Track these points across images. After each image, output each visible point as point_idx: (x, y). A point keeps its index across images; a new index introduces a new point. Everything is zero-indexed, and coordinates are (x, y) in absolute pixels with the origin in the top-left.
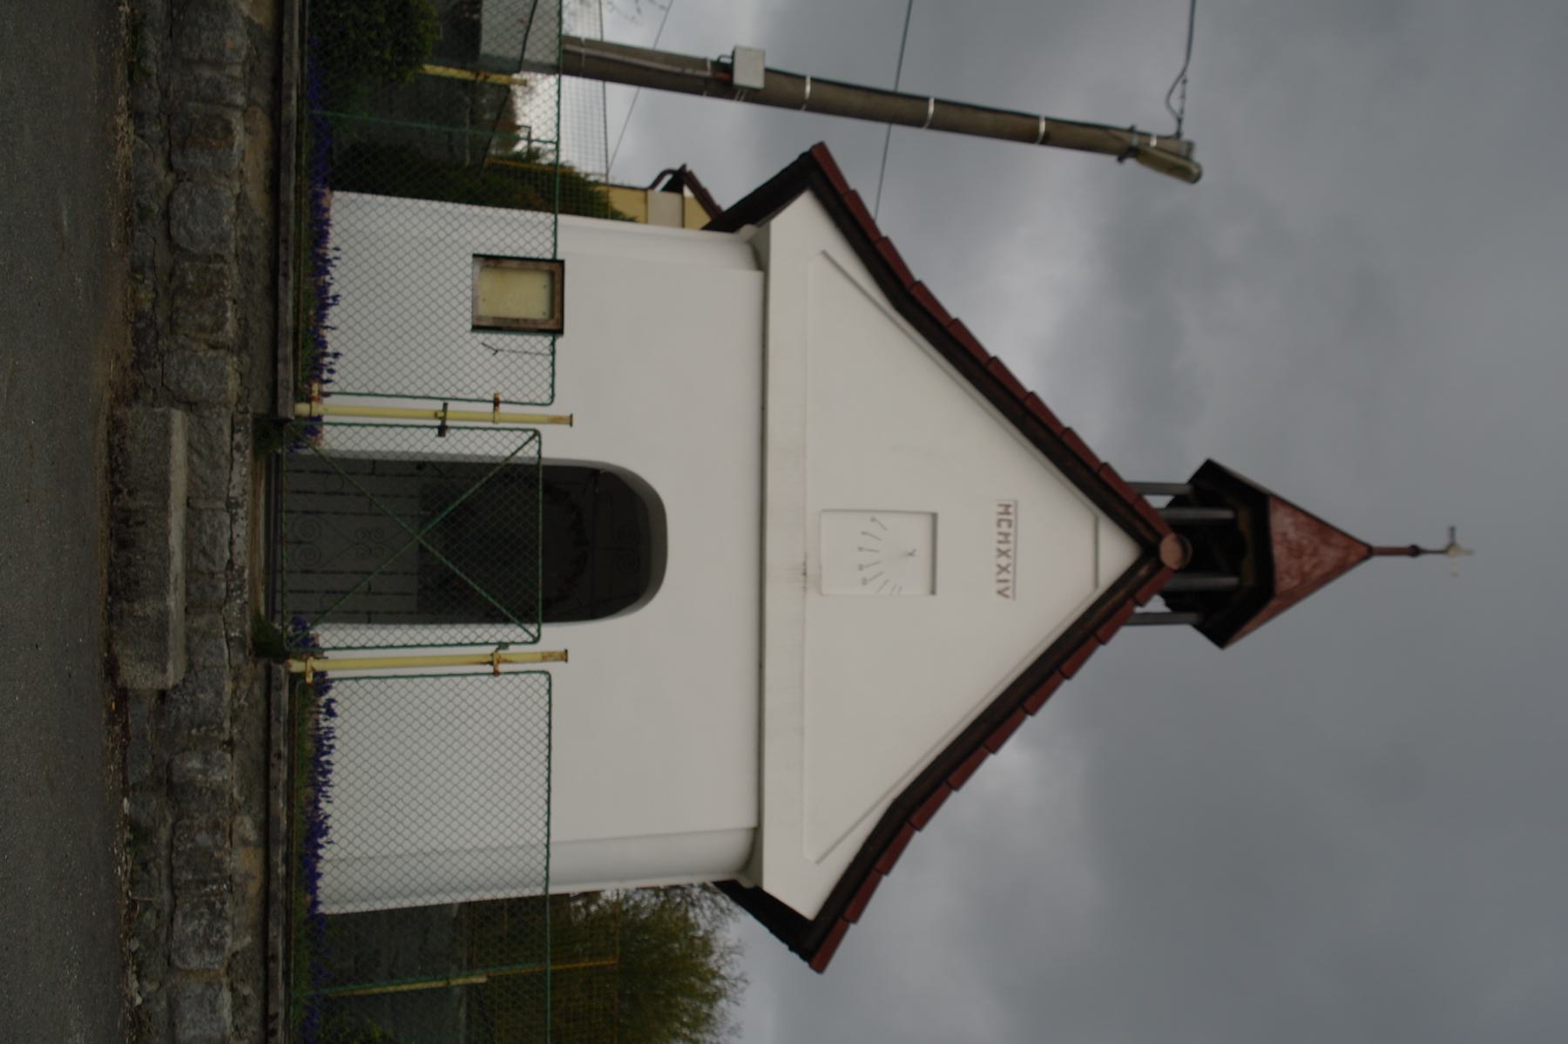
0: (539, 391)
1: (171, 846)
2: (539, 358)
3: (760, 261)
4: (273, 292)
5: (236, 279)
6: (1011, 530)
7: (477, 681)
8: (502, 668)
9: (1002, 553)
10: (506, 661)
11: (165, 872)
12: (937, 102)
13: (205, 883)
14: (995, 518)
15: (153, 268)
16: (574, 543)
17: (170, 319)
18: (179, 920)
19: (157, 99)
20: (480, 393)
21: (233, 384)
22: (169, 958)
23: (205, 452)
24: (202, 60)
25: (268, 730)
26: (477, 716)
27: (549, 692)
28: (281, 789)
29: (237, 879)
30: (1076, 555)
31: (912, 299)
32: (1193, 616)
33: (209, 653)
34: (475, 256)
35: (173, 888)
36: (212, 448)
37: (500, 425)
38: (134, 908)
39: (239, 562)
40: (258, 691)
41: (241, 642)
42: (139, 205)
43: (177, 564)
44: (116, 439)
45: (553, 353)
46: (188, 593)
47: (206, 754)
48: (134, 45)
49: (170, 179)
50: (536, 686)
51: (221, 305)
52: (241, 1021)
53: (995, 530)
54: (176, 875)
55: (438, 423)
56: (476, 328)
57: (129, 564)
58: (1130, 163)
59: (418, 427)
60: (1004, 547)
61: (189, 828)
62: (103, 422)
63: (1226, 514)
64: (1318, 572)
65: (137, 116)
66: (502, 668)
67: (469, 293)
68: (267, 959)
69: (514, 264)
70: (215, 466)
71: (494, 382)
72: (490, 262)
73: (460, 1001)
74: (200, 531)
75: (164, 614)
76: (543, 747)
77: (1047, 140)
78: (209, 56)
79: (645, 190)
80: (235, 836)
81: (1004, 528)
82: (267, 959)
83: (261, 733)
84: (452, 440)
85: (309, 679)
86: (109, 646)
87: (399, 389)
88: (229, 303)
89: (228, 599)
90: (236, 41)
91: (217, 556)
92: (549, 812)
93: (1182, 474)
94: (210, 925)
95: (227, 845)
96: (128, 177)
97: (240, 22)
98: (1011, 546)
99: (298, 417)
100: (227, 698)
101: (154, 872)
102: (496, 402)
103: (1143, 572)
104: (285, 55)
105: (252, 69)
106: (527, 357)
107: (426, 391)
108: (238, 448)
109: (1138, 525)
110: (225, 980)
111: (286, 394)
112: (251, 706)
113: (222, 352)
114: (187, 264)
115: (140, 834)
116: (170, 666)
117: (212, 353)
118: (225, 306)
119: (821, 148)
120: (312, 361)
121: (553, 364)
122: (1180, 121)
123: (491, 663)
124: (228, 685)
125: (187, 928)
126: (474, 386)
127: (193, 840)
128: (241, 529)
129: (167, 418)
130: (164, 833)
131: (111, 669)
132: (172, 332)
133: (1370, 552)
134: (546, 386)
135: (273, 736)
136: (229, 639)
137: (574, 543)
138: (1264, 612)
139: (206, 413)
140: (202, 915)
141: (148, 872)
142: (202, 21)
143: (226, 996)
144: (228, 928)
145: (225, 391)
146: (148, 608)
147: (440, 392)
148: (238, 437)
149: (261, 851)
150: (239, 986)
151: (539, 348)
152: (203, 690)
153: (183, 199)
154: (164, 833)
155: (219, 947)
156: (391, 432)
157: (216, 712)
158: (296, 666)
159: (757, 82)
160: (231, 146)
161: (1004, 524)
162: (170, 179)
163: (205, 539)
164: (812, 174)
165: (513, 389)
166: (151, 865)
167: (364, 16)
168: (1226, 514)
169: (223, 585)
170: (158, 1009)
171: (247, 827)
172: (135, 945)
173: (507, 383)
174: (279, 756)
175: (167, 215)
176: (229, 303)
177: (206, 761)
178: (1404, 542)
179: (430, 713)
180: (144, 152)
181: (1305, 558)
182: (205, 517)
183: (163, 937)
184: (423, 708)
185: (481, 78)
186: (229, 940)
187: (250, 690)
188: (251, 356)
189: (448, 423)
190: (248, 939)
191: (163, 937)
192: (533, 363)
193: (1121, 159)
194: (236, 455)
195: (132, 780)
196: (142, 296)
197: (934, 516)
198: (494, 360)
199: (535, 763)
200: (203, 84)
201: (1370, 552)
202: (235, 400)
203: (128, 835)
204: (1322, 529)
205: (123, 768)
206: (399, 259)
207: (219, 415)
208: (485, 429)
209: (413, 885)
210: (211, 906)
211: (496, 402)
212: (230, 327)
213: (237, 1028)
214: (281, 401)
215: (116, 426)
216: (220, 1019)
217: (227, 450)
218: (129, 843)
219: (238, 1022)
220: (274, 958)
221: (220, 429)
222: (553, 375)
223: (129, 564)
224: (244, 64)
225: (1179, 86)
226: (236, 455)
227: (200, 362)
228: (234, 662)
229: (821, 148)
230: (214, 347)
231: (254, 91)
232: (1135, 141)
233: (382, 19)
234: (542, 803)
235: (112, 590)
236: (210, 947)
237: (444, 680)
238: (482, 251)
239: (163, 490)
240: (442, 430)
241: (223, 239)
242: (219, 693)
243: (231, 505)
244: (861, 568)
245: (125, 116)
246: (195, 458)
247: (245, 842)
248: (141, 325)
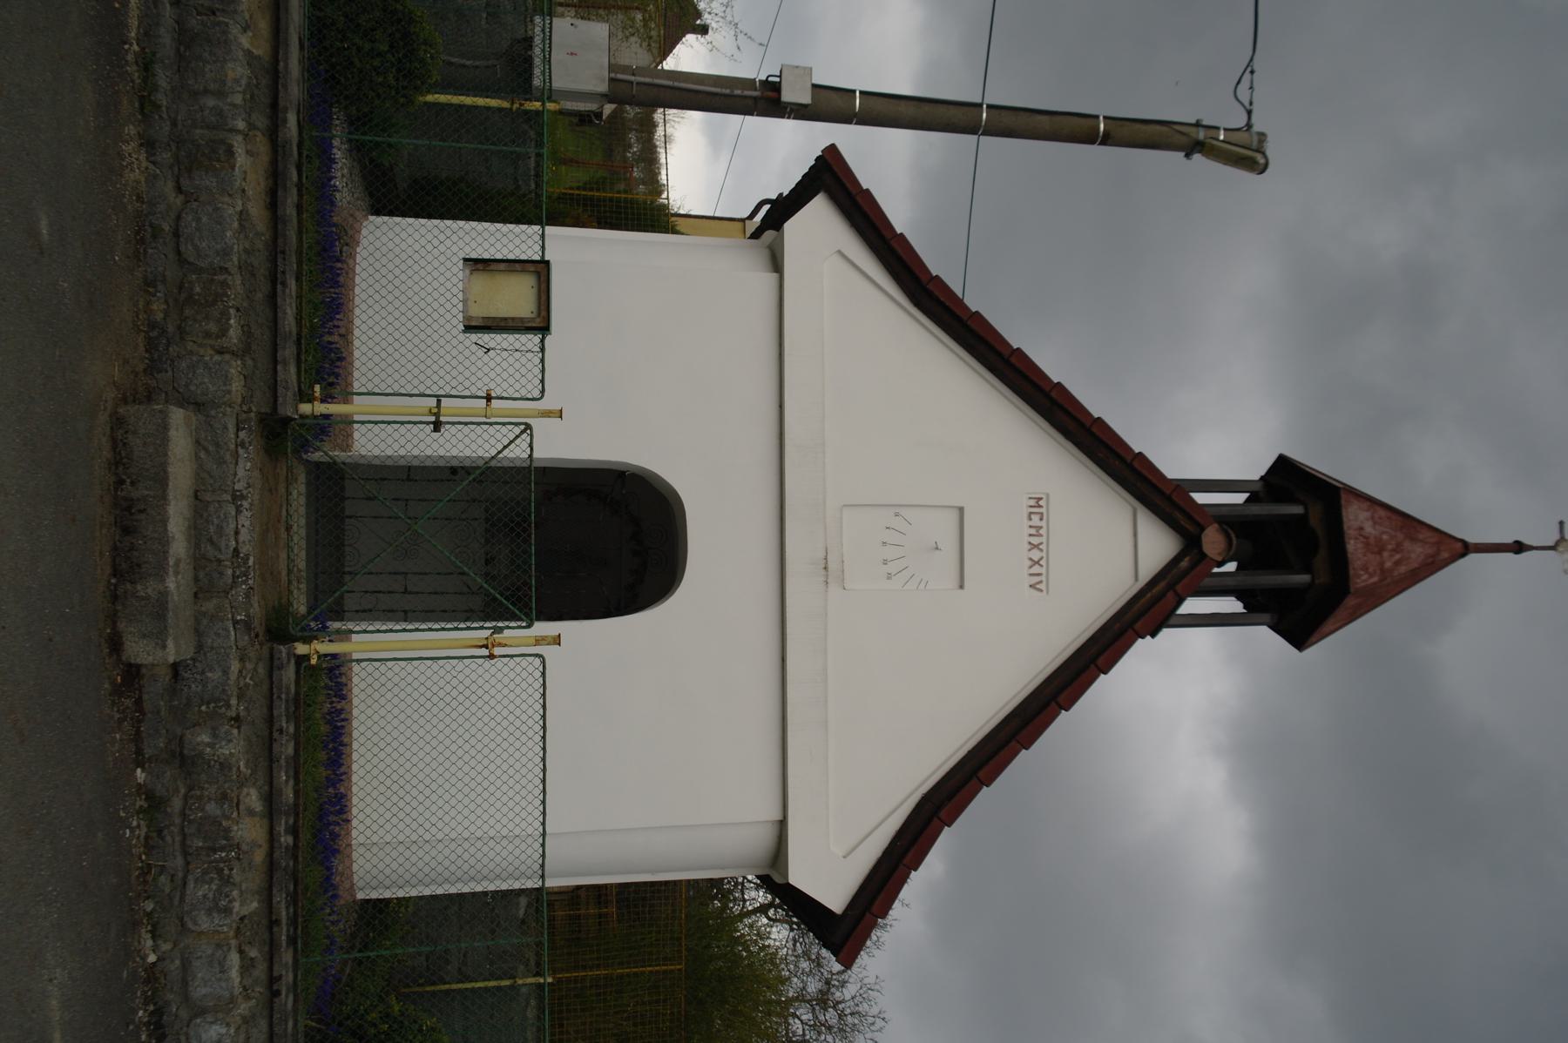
1: (183, 815)
2: (530, 355)
4: (272, 299)
5: (240, 289)
6: (1043, 523)
7: (473, 664)
8: (497, 651)
9: (1034, 546)
10: (500, 645)
11: (178, 839)
12: (989, 106)
13: (215, 851)
14: (1026, 511)
15: (164, 281)
16: (598, 543)
17: (179, 327)
18: (191, 885)
19: (167, 128)
20: (474, 390)
21: (237, 386)
22: (182, 920)
24: (206, 91)
25: (271, 708)
27: (543, 674)
28: (283, 762)
29: (244, 847)
30: (1116, 548)
31: (930, 294)
32: (1266, 617)
34: (466, 260)
35: (185, 854)
36: (217, 445)
38: (149, 872)
39: (244, 550)
40: (261, 670)
41: (247, 625)
42: (151, 225)
43: (179, 547)
45: (543, 350)
46: (196, 579)
47: (214, 729)
50: (531, 669)
51: (225, 315)
52: (248, 982)
53: (1027, 523)
55: (433, 419)
56: (469, 329)
57: (132, 548)
59: (415, 423)
60: (1035, 541)
61: (200, 798)
62: (103, 418)
63: (1297, 510)
64: (1403, 569)
65: (149, 144)
66: (497, 651)
67: (460, 296)
68: (273, 923)
69: (502, 266)
70: (221, 462)
72: (478, 265)
74: (207, 521)
75: (164, 594)
77: (1107, 140)
78: (212, 86)
79: (743, 220)
80: (242, 807)
81: (1036, 520)
83: (265, 710)
85: (314, 661)
86: (114, 623)
88: (232, 311)
89: (234, 584)
90: (237, 71)
92: (544, 791)
93: (1254, 468)
94: (219, 890)
95: (235, 814)
96: (139, 198)
97: (241, 53)
98: (1044, 539)
99: (302, 417)
100: (233, 677)
101: (169, 839)
102: (489, 398)
103: (1184, 564)
105: (252, 97)
106: (518, 355)
107: (422, 389)
108: (242, 445)
109: (1179, 516)
110: (233, 942)
112: (256, 685)
113: (227, 357)
115: (154, 803)
117: (217, 358)
119: (832, 150)
121: (542, 361)
122: (1249, 113)
124: (234, 667)
125: (199, 892)
127: (203, 810)
128: (245, 519)
129: (164, 415)
130: (177, 803)
131: (115, 644)
132: (182, 339)
133: (1466, 549)
135: (275, 713)
136: (235, 622)
137: (598, 543)
138: (1341, 612)
139: (213, 413)
141: (163, 839)
143: (234, 958)
144: (235, 893)
145: (229, 392)
146: (148, 588)
147: (435, 390)
148: (242, 434)
149: (266, 822)
150: (246, 948)
151: (530, 346)
154: (177, 803)
155: (227, 911)
156: (389, 429)
158: (301, 649)
159: (805, 98)
160: (233, 168)
161: (1035, 518)
162: (179, 200)
163: (212, 529)
164: (828, 177)
165: (505, 385)
167: (367, 46)
168: (1297, 510)
169: (230, 572)
171: (253, 798)
172: (149, 906)
173: (499, 380)
174: (281, 731)
175: (176, 234)
176: (232, 311)
177: (215, 736)
178: (1509, 540)
179: (429, 694)
180: (155, 176)
181: (1386, 554)
182: (211, 509)
183: (176, 902)
184: (422, 689)
185: (516, 106)
186: (237, 904)
187: (255, 669)
189: (442, 419)
190: (255, 904)
191: (176, 902)
192: (524, 360)
193: (1188, 156)
194: (241, 451)
195: (148, 752)
196: (155, 307)
197: (961, 510)
199: (530, 743)
201: (1466, 549)
204: (1408, 524)
206: (411, 272)
208: (479, 424)
209: (447, 874)
211: (489, 398)
212: (234, 333)
213: (245, 989)
214: (280, 400)
215: (118, 422)
219: (245, 982)
220: (277, 922)
223: (132, 548)
224: (244, 93)
225: (1247, 75)
226: (241, 451)
228: (240, 644)
229: (832, 150)
230: (220, 352)
231: (254, 116)
232: (1201, 135)
233: (384, 47)
234: (538, 781)
236: (219, 911)
237: (441, 662)
238: (474, 256)
239: (162, 480)
240: (437, 426)
241: (226, 253)
242: (226, 672)
243: (237, 497)
244: (885, 562)
246: (202, 455)
247: (251, 813)
248: (154, 334)
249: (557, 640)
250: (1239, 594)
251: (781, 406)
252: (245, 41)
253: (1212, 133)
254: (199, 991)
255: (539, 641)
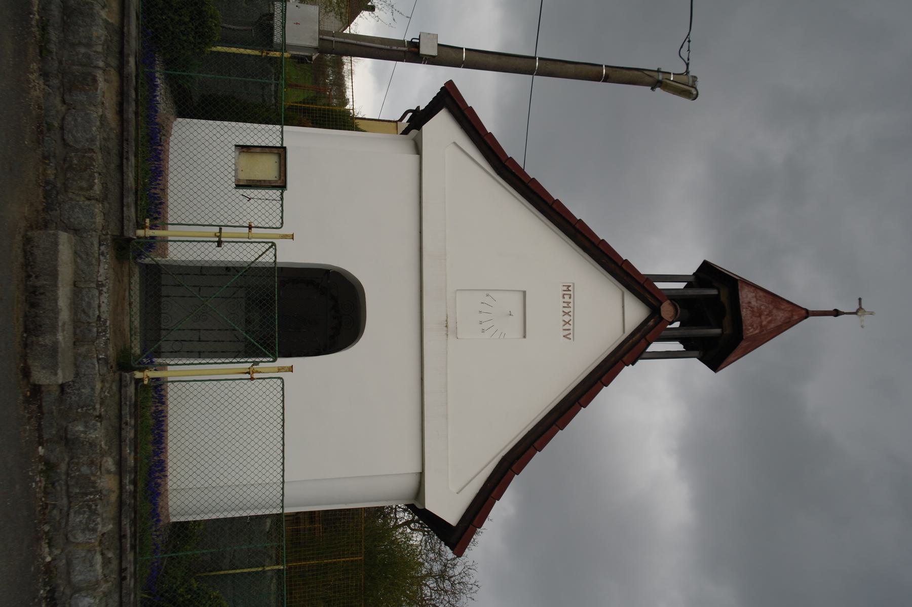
0: (274, 221)
1: (67, 474)
2: (274, 202)
3: (418, 149)
4: (120, 168)
5: (101, 162)
8: (255, 376)
9: (566, 313)
11: (64, 488)
13: (86, 494)
14: (561, 293)
15: (54, 156)
16: (313, 311)
18: (72, 515)
19: (56, 64)
20: (241, 223)
21: (99, 219)
22: (66, 535)
23: (84, 256)
24: (80, 44)
25: (120, 410)
26: (241, 403)
29: (104, 492)
30: (612, 313)
31: (506, 168)
32: (696, 353)
33: (88, 366)
34: (236, 146)
35: (69, 497)
36: (87, 254)
37: (253, 240)
38: (46, 508)
39: (104, 316)
40: (115, 388)
41: (106, 361)
43: (65, 315)
44: (28, 247)
46: (75, 334)
47: (86, 422)
48: (43, 36)
49: (63, 108)
50: (275, 386)
51: (92, 176)
53: (562, 300)
54: (70, 490)
55: (217, 239)
58: (658, 90)
60: (567, 310)
61: (77, 464)
62: (19, 238)
63: (714, 292)
64: (772, 326)
65: (45, 75)
66: (255, 376)
68: (122, 537)
69: (258, 150)
71: (249, 217)
72: (244, 149)
73: (272, 579)
75: (56, 343)
76: (279, 420)
77: (607, 79)
78: (84, 41)
79: (396, 122)
80: (103, 469)
81: (567, 299)
82: (122, 537)
84: (225, 249)
85: (146, 382)
86: (26, 360)
87: (195, 221)
88: (96, 175)
89: (98, 337)
90: (99, 32)
91: (91, 314)
93: (690, 268)
94: (89, 518)
95: (98, 473)
97: (101, 21)
98: (571, 309)
99: (139, 238)
100: (97, 391)
101: (58, 488)
102: (250, 227)
103: (651, 323)
104: (126, 38)
106: (267, 202)
107: (210, 221)
108: (103, 254)
109: (647, 295)
110: (98, 549)
111: (129, 225)
112: (111, 396)
113: (93, 202)
114: (73, 154)
115: (50, 467)
116: (60, 372)
117: (87, 202)
118: (94, 177)
119: (450, 84)
120: (153, 207)
121: (282, 205)
122: (688, 65)
123: (249, 373)
124: (98, 385)
125: (76, 519)
126: (237, 219)
127: (79, 471)
128: (104, 298)
129: (56, 236)
130: (63, 467)
131: (26, 373)
132: (66, 191)
133: (807, 314)
134: (278, 218)
135: (123, 413)
136: (99, 359)
137: (313, 311)
139: (85, 235)
140: (85, 512)
142: (80, 22)
143: (98, 558)
144: (99, 520)
145: (95, 223)
146: (47, 340)
147: (218, 222)
148: (103, 248)
149: (117, 477)
150: (106, 552)
151: (274, 196)
152: (84, 387)
153: (70, 119)
154: (63, 467)
155: (94, 530)
157: (92, 400)
158: (138, 375)
159: (434, 52)
160: (96, 89)
161: (567, 297)
162: (64, 108)
164: (448, 99)
166: (56, 484)
168: (714, 292)
169: (95, 330)
170: (61, 564)
171: (109, 463)
172: (47, 528)
174: (126, 423)
175: (62, 128)
176: (96, 175)
177: (86, 427)
178: (831, 309)
180: (49, 94)
182: (84, 292)
183: (63, 524)
186: (100, 527)
187: (111, 387)
188: (109, 203)
191: (63, 524)
194: (102, 258)
195: (46, 437)
196: (49, 172)
197: (524, 292)
198: (248, 204)
200: (80, 56)
201: (807, 314)
202: (100, 228)
203: (41, 467)
205: (39, 429)
206: (203, 154)
207: (92, 236)
208: (244, 242)
210: (90, 507)
211: (250, 227)
212: (97, 188)
214: (125, 228)
215: (27, 240)
216: (95, 571)
217: (96, 255)
218: (42, 471)
220: (125, 536)
221: (92, 244)
222: (282, 212)
224: (103, 45)
226: (102, 258)
227: (81, 208)
228: (102, 372)
229: (450, 84)
230: (89, 199)
232: (661, 77)
233: (187, 19)
234: (279, 452)
235: (26, 330)
236: (89, 530)
238: (241, 143)
240: (219, 243)
241: (92, 140)
242: (93, 389)
243: (99, 285)
245: (36, 75)
246: (79, 260)
247: (109, 472)
248: (48, 188)
249: (291, 369)
250: (682, 340)
251: (421, 232)
252: (103, 14)
253: (666, 76)
254: (77, 578)
255: (280, 370)
